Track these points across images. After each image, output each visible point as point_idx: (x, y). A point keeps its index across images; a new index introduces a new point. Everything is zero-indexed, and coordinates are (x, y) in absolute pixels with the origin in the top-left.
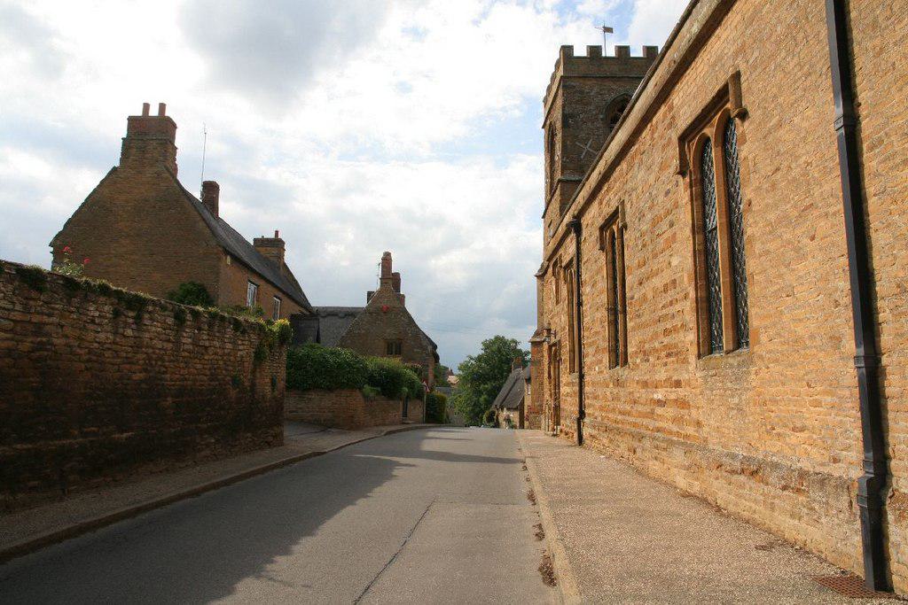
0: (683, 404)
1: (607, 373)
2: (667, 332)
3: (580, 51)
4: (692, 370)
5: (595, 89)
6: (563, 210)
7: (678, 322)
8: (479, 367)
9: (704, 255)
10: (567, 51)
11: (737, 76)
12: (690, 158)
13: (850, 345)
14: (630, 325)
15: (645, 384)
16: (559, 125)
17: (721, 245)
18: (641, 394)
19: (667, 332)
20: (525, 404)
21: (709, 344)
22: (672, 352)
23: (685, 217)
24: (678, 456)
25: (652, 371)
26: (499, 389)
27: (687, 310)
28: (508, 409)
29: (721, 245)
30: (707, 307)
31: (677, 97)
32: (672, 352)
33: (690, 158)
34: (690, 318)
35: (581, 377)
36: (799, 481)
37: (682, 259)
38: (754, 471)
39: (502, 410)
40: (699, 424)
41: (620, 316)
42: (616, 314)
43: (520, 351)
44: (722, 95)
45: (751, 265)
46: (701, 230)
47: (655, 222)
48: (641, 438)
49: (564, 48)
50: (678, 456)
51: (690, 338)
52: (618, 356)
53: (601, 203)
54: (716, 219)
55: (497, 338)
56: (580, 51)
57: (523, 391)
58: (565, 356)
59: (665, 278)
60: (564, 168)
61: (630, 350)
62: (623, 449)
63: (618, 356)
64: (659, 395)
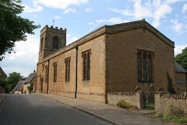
0: (63, 87)
1: (53, 83)
2: (62, 79)
3: (49, 27)
4: (64, 83)
5: (52, 34)
6: (45, 57)
7: (63, 78)
8: (8, 80)
9: (66, 72)
10: (47, 26)
11: (70, 57)
12: (66, 61)
13: (75, 82)
14: (57, 77)
15: (59, 85)
16: (44, 38)
17: (68, 72)
18: (58, 86)
19: (62, 79)
20: (24, 89)
21: (66, 81)
22: (62, 81)
23: (65, 67)
24: (62, 92)
25: (60, 83)
26: (15, 86)
27: (64, 77)
28: (18, 91)
29: (68, 72)
30: (66, 77)
31: (66, 54)
32: (62, 81)
33: (66, 61)
34: (64, 78)
35: (48, 84)
36: (99, 95)
37: (64, 71)
38: (69, 92)
39: (16, 91)
40: (65, 89)
41: (56, 76)
42: (55, 75)
43: (21, 76)
44: (69, 58)
45: (70, 74)
46: (66, 69)
47: (61, 66)
48: (58, 91)
49: (46, 25)
50: (62, 92)
51: (64, 80)
52: (55, 81)
53: (53, 60)
54: (68, 69)
55: (14, 73)
56: (49, 27)
57: (23, 86)
58: (44, 80)
59: (62, 73)
60: (45, 47)
61: (57, 80)
62: (55, 93)
63: (55, 81)
64: (60, 86)
